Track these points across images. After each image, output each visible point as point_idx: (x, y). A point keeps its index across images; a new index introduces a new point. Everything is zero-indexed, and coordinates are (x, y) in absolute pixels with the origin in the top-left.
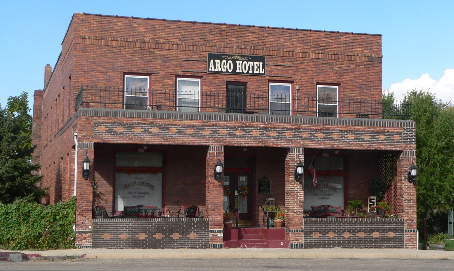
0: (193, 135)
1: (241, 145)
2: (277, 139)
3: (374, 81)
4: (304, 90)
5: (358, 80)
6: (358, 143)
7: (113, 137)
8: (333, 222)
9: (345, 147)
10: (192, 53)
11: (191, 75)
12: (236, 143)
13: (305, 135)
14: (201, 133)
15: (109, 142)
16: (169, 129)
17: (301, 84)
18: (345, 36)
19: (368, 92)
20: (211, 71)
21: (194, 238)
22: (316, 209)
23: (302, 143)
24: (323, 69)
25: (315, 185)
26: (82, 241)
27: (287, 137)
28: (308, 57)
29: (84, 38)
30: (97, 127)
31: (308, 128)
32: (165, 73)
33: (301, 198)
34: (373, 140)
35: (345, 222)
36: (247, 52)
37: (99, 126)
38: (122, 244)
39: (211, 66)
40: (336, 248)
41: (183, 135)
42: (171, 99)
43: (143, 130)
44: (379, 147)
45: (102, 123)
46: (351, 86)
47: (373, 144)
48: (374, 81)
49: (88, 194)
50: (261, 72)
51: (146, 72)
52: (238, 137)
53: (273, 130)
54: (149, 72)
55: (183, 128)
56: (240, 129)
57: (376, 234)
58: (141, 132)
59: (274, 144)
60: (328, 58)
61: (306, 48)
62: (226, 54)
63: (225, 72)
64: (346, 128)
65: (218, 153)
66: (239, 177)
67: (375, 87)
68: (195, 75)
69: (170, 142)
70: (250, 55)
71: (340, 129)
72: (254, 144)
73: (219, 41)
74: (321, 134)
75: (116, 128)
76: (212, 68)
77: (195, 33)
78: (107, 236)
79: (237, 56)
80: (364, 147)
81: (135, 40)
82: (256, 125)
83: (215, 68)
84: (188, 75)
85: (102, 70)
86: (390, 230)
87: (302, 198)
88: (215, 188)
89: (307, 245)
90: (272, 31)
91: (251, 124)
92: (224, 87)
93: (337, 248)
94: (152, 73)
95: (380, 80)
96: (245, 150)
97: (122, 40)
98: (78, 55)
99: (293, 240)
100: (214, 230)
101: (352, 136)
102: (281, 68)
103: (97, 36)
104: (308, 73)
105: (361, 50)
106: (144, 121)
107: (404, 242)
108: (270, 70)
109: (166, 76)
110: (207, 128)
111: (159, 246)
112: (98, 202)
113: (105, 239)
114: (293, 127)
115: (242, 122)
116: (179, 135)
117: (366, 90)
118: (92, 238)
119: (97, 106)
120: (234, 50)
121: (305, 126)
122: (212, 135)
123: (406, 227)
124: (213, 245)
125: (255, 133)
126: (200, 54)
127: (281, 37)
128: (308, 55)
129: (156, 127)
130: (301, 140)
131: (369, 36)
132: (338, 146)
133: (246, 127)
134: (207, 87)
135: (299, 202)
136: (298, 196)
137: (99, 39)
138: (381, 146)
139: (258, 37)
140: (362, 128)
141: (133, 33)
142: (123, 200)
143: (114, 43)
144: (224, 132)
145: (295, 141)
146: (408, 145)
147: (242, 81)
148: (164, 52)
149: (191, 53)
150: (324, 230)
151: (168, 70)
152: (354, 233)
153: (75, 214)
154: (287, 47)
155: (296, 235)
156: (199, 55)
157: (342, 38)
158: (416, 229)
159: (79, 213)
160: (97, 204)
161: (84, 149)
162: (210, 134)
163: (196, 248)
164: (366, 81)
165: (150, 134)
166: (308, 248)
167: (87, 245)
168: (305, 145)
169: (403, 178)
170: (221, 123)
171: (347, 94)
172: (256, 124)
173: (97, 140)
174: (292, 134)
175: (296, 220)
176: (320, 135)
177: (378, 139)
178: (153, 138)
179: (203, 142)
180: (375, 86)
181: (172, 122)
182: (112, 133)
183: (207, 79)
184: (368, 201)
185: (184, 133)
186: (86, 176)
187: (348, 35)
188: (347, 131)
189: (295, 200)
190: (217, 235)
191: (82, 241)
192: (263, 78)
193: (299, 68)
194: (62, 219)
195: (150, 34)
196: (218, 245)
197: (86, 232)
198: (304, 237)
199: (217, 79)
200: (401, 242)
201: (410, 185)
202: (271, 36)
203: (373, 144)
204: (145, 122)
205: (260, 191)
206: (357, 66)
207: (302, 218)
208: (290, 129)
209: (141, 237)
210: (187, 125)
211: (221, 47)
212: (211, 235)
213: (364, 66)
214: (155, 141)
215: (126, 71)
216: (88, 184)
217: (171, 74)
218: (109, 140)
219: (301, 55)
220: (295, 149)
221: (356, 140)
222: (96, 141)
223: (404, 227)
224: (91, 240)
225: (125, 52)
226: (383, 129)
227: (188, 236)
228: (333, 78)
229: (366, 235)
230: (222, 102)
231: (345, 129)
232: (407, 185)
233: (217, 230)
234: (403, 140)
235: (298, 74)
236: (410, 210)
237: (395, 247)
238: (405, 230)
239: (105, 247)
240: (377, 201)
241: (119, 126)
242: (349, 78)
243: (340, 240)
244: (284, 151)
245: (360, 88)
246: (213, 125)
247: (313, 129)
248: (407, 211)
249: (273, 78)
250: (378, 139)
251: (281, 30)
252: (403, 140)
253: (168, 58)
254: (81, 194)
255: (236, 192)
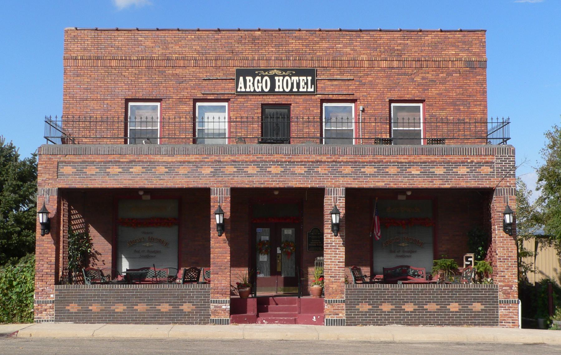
0: (188, 175)
1: (255, 186)
2: (305, 176)
3: (476, 94)
4: (371, 111)
5: (451, 94)
6: (426, 179)
7: (82, 180)
8: (389, 289)
9: (407, 184)
10: (215, 70)
11: (213, 98)
12: (247, 184)
13: (348, 170)
14: (199, 172)
15: (77, 186)
16: (156, 168)
17: (367, 103)
18: (430, 36)
19: (466, 109)
20: (241, 92)
21: (189, 310)
22: (389, 271)
23: (342, 181)
24: (398, 81)
25: (378, 239)
26: (42, 313)
27: (320, 174)
28: (376, 66)
29: (76, 59)
30: (61, 168)
31: (351, 160)
32: (179, 97)
33: (341, 257)
34: (448, 175)
35: (407, 289)
36: (289, 64)
37: (64, 167)
38: (92, 318)
39: (240, 86)
40: (393, 325)
41: (175, 175)
42: (188, 130)
43: (120, 170)
44: (458, 184)
45: (68, 163)
46: (440, 103)
47: (450, 179)
48: (476, 94)
49: (50, 253)
50: (309, 90)
51: (154, 98)
52: (250, 176)
53: (301, 165)
54: (158, 98)
55: (175, 165)
56: (254, 165)
57: (454, 307)
58: (119, 172)
59: (302, 184)
60: (406, 66)
61: (374, 54)
62: (261, 68)
63: (259, 92)
64: (407, 159)
65: (222, 197)
66: (283, 229)
67: (476, 103)
68: (219, 98)
69: (156, 184)
70: (295, 68)
71: (399, 160)
72: (273, 184)
73: (251, 51)
74: (371, 168)
75: (87, 168)
76: (241, 87)
77: (219, 43)
78: (73, 308)
79: (275, 70)
80: (435, 184)
81: (141, 57)
82: (275, 160)
83: (245, 87)
84: (210, 98)
85: (98, 97)
86: (476, 300)
87: (343, 257)
88: (217, 245)
89: (350, 321)
90: (325, 35)
91: (268, 158)
92: (259, 111)
93: (396, 325)
94: (162, 97)
95: (485, 92)
96: (276, 193)
97: (124, 58)
98: (68, 80)
99: (330, 315)
100: (216, 301)
101: (417, 170)
102: (338, 83)
103: (92, 55)
104: (377, 88)
105: (454, 52)
106: (123, 158)
107: (498, 317)
108: (322, 87)
109: (181, 101)
110: (208, 165)
111: (142, 320)
112: (93, 263)
113: (72, 310)
114: (329, 160)
115: (257, 156)
116: (169, 175)
117: (462, 107)
118: (54, 309)
119: (92, 143)
120: (272, 63)
121: (347, 158)
122: (214, 174)
123: (501, 296)
124: (216, 320)
125: (275, 170)
126: (227, 70)
127: (338, 41)
128: (376, 63)
129: (139, 166)
130: (341, 177)
131: (466, 33)
132: (396, 184)
133: (261, 161)
134: (236, 113)
135: (339, 262)
136: (337, 254)
137: (94, 59)
138: (461, 182)
139: (305, 43)
140: (433, 158)
141: (138, 49)
142: (128, 261)
143: (114, 63)
144: (231, 169)
145: (333, 179)
146: (503, 179)
147: (283, 103)
148: (178, 71)
149: (214, 70)
150: (82, 300)
151: (183, 93)
152: (420, 304)
153: (33, 279)
154: (347, 54)
155: (333, 307)
156: (225, 72)
157: (426, 38)
158: (517, 299)
159: (37, 278)
160: (93, 266)
161: (45, 196)
162: (211, 172)
163: (192, 323)
164: (463, 94)
165: (131, 175)
166: (352, 325)
167: (48, 318)
168: (346, 184)
169: (496, 227)
170: (227, 158)
171: (434, 113)
172: (276, 157)
173: (61, 185)
174: (327, 170)
175: (335, 286)
176: (369, 170)
177: (457, 172)
178: (134, 180)
179: (200, 183)
180: (476, 101)
181: (160, 158)
182: (80, 175)
183: (235, 102)
184: (464, 259)
185: (177, 172)
186: (335, 231)
187: (434, 34)
188: (409, 162)
189: (332, 259)
190: (221, 307)
191: (42, 313)
192: (313, 98)
193: (364, 81)
194: (20, 286)
195: (159, 49)
196: (223, 319)
197: (46, 303)
198: (346, 310)
199: (249, 102)
200: (493, 317)
201: (506, 237)
202: (323, 41)
203: (450, 179)
204: (124, 160)
205: (309, 247)
206: (449, 74)
207: (343, 284)
208: (325, 162)
209: (118, 308)
210: (180, 162)
211: (253, 59)
212: (213, 307)
213: (460, 74)
214: (137, 184)
215: (129, 97)
216: (49, 240)
217: (187, 97)
218: (77, 184)
219: (366, 64)
220: (331, 189)
221: (424, 175)
222: (60, 186)
223: (497, 297)
224: (53, 312)
225: (128, 74)
226: (465, 159)
227: (181, 308)
228: (413, 93)
229: (438, 307)
230: (256, 129)
231: (406, 161)
232: (502, 237)
233: (221, 300)
234: (495, 173)
235: (363, 90)
236: (508, 272)
237: (483, 324)
238: (500, 301)
239: (71, 321)
240: (476, 259)
241: (91, 166)
242: (438, 92)
243: (399, 315)
244: (205, 192)
245: (454, 104)
246: (216, 161)
247: (359, 162)
248: (502, 274)
249: (327, 97)
250: (457, 172)
251: (337, 33)
252: (495, 173)
253: (184, 78)
254: (41, 254)
255: (278, 249)
